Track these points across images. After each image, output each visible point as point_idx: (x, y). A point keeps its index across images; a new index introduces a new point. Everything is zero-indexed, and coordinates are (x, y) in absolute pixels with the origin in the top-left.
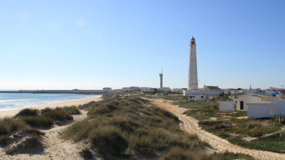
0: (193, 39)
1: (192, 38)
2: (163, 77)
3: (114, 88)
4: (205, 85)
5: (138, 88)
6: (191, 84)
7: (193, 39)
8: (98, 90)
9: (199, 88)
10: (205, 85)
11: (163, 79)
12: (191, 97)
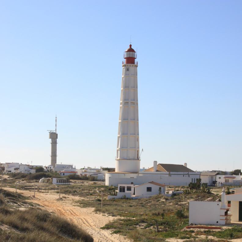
0: (131, 50)
1: (129, 47)
2: (58, 140)
4: (155, 162)
6: (123, 159)
7: (131, 50)
9: (141, 167)
10: (155, 162)
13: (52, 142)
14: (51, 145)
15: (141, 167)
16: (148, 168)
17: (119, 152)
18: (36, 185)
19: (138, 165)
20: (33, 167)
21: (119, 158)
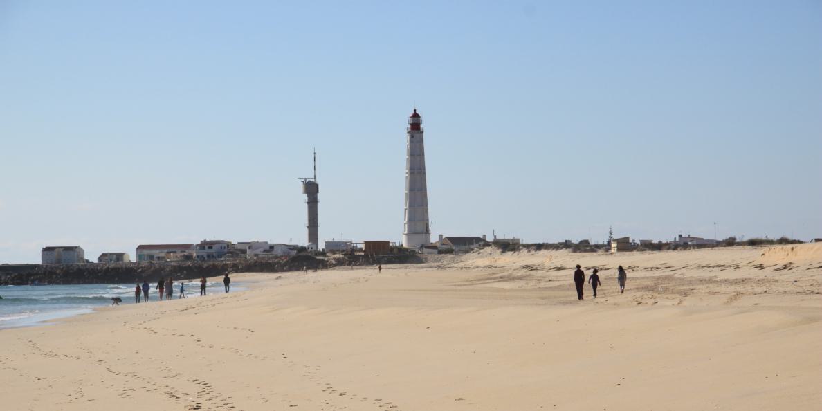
0: (416, 116)
1: (413, 112)
2: (319, 196)
3: (234, 242)
4: (441, 236)
5: (229, 245)
6: (411, 233)
7: (416, 116)
8: (70, 286)
9: (96, 261)
10: (441, 236)
11: (319, 205)
12: (620, 249)
13: (309, 200)
14: (306, 206)
15: (96, 261)
16: (577, 242)
17: (406, 225)
18: (47, 355)
19: (428, 238)
20: (272, 247)
21: (406, 232)
